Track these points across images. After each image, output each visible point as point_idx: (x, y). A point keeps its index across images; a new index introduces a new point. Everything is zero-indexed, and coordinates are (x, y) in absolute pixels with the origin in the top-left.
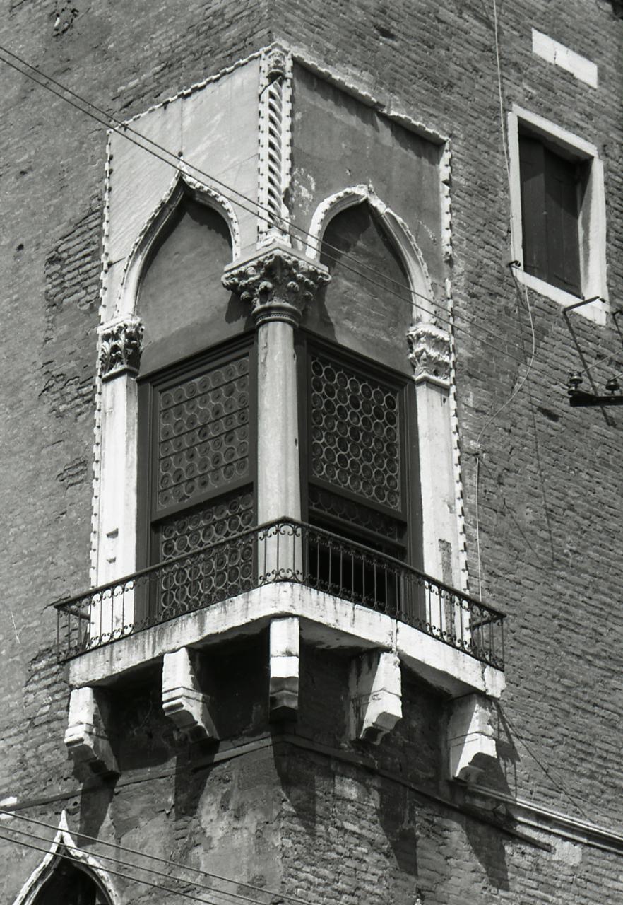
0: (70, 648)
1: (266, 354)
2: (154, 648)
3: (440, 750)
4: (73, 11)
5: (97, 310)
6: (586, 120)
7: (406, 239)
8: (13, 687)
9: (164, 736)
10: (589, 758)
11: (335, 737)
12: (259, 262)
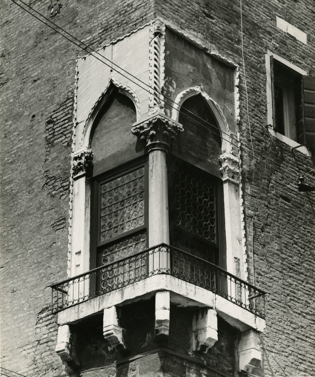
0: (58, 307)
1: (153, 166)
2: (99, 306)
3: (235, 357)
4: (60, 5)
5: (71, 145)
6: (302, 59)
7: (219, 112)
8: (30, 326)
9: (104, 349)
10: (304, 362)
11: (185, 350)
12: (150, 121)
